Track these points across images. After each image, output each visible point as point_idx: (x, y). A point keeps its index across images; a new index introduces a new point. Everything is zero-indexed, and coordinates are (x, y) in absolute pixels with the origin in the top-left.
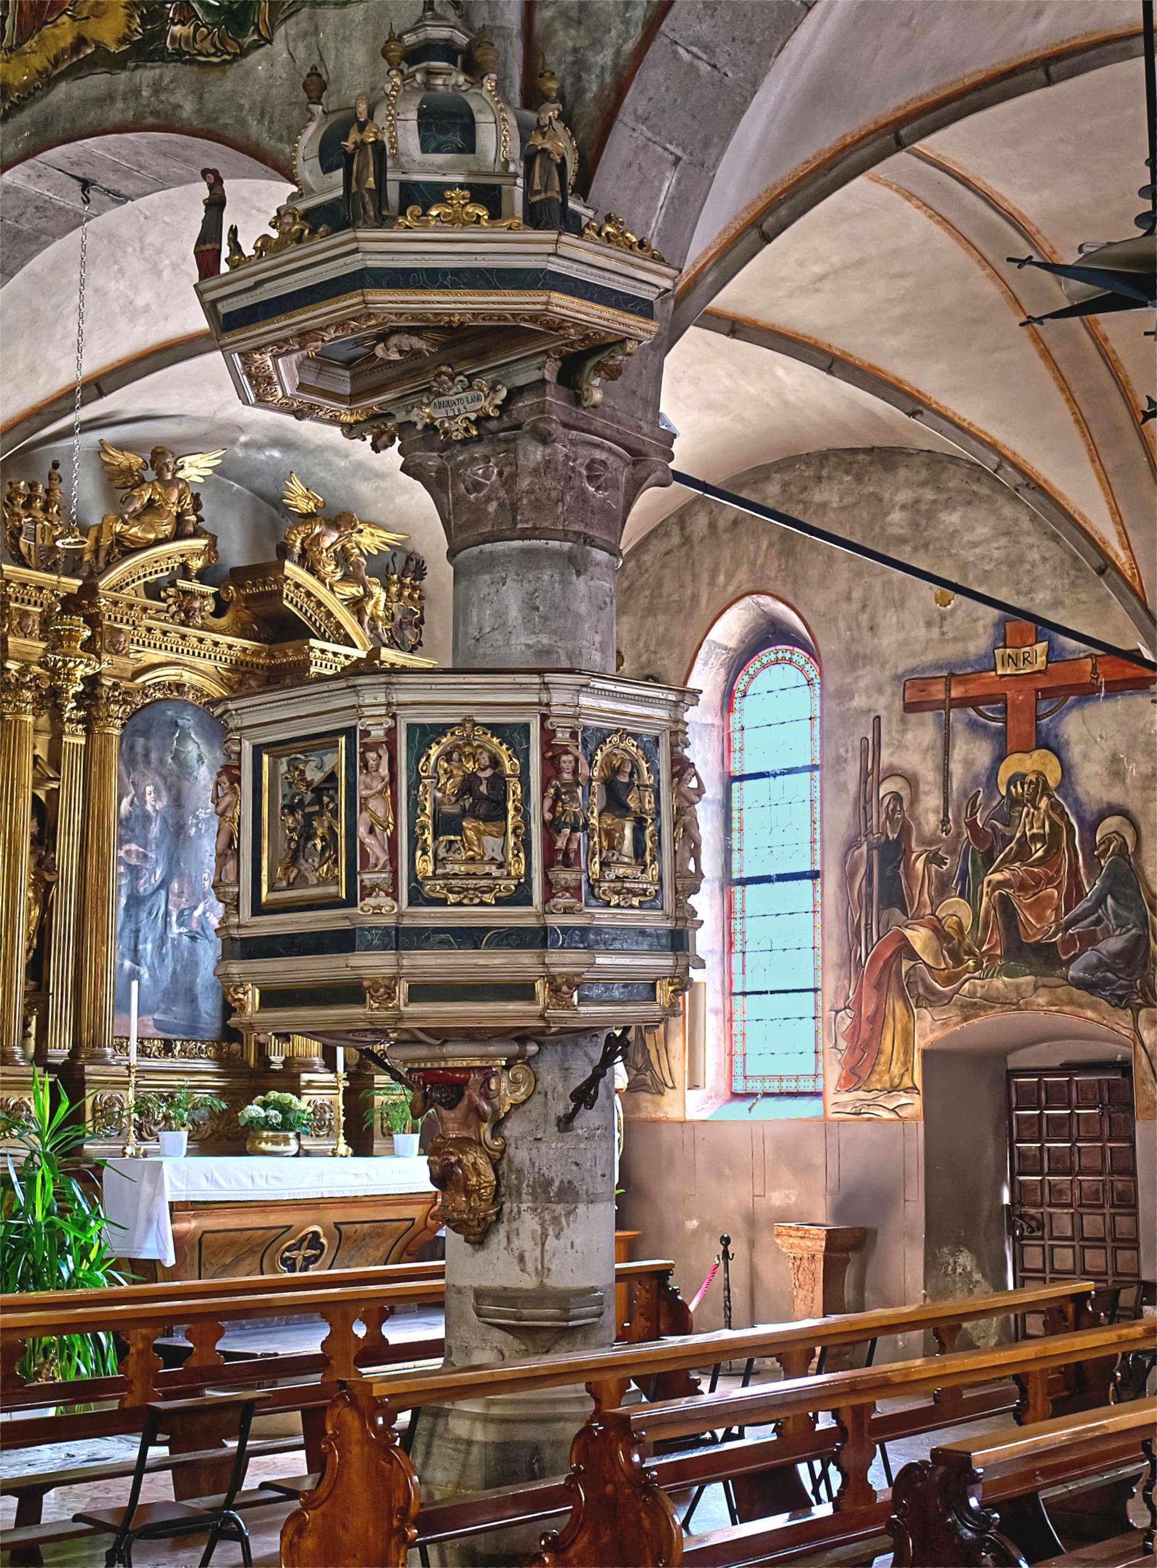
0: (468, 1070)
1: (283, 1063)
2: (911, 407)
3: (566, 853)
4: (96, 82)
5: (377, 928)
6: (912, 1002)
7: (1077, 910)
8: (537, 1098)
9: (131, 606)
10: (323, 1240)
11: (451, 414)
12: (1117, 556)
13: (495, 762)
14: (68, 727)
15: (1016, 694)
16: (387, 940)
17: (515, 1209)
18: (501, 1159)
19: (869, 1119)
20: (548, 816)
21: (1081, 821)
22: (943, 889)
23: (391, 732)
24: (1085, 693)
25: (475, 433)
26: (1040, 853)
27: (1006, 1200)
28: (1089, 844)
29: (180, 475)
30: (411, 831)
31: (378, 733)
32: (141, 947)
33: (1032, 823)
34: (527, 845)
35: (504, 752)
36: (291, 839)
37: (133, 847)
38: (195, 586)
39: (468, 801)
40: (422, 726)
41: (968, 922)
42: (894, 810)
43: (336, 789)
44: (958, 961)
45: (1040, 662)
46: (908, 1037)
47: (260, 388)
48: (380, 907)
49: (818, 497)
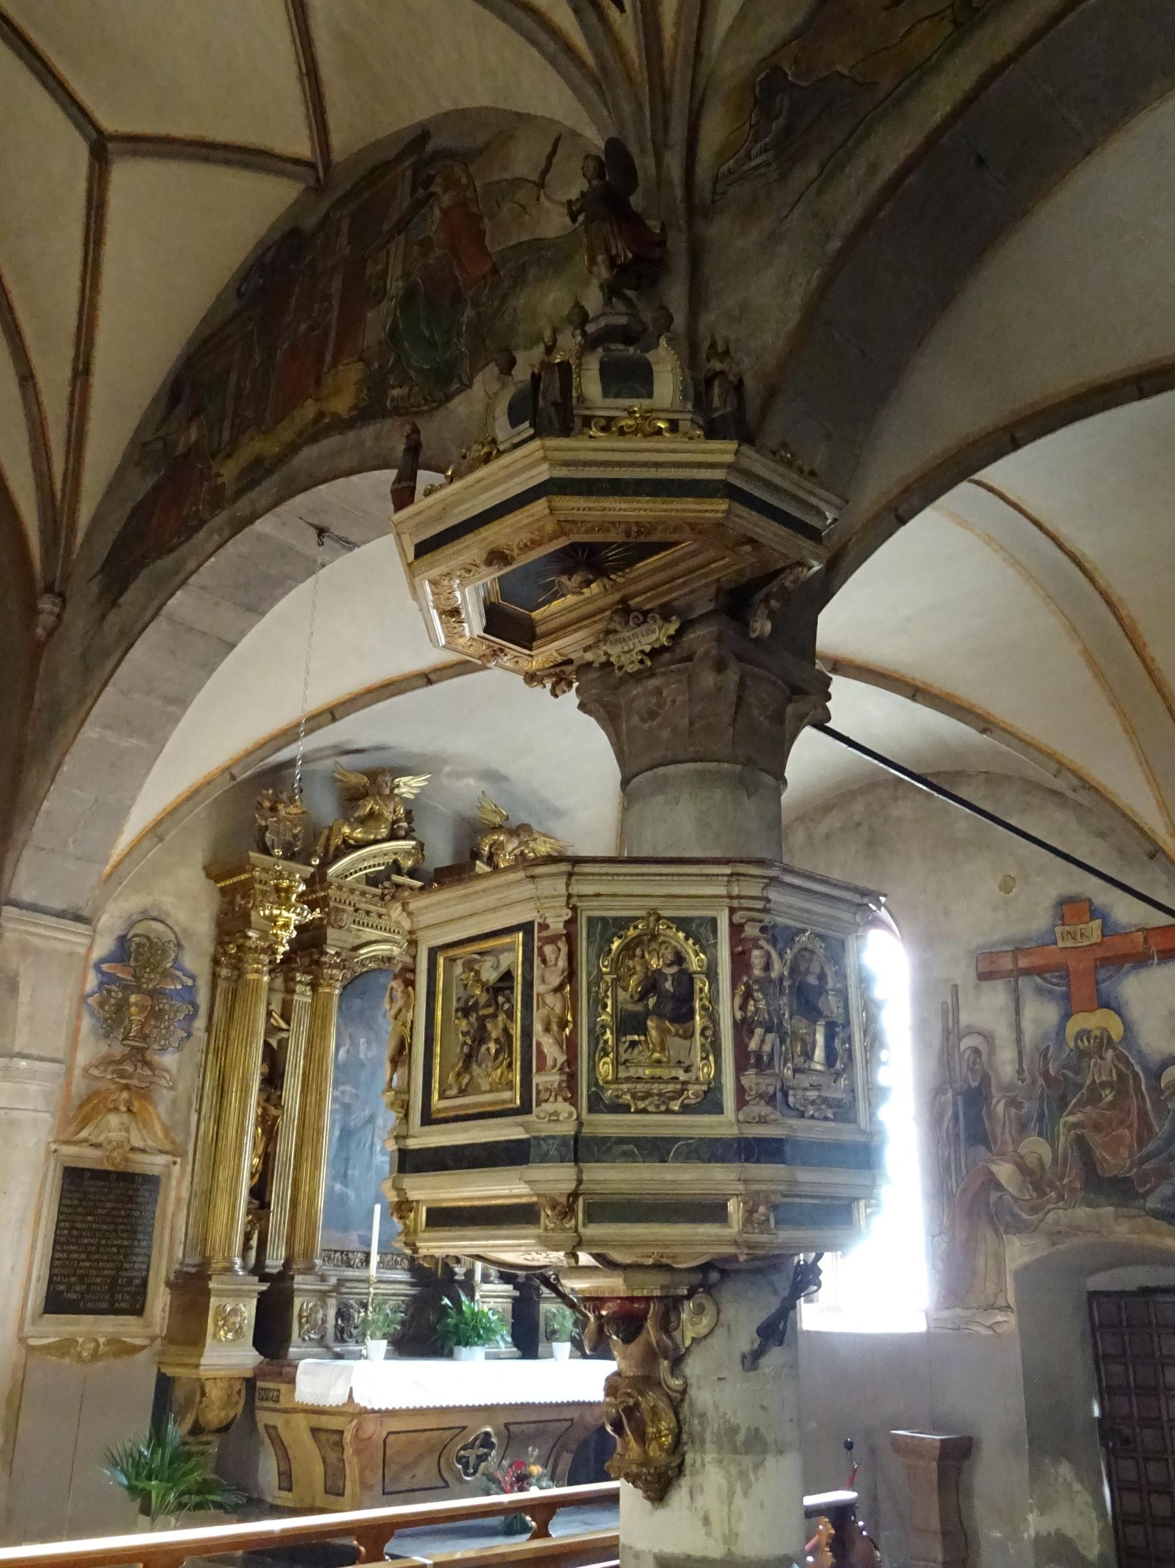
0: (648, 1299)
1: (465, 1274)
2: (982, 725)
3: (759, 1057)
4: (330, 443)
5: (554, 1137)
6: (1002, 1230)
7: (1150, 1147)
8: (720, 1332)
9: (352, 891)
10: (494, 1440)
11: (626, 649)
12: (1165, 842)
13: (679, 959)
14: (299, 988)
15: (1076, 966)
16: (564, 1150)
17: (698, 1463)
18: (682, 1400)
19: (969, 1334)
20: (739, 1015)
21: (1145, 1069)
22: (1023, 1128)
23: (570, 923)
24: (1140, 960)
25: (649, 663)
26: (1110, 1098)
27: (1096, 1412)
28: (1155, 1089)
29: (396, 791)
30: (591, 1031)
31: (557, 925)
32: (350, 1172)
33: (1100, 1070)
34: (715, 1047)
35: (689, 948)
36: (465, 1043)
37: (348, 1088)
38: (405, 880)
39: (652, 1001)
40: (604, 920)
41: (1047, 1158)
42: (974, 1062)
43: (511, 989)
44: (1042, 1193)
45: (1096, 937)
46: (999, 1259)
47: (541, 1488)
48: (556, 1113)
49: (896, 812)
